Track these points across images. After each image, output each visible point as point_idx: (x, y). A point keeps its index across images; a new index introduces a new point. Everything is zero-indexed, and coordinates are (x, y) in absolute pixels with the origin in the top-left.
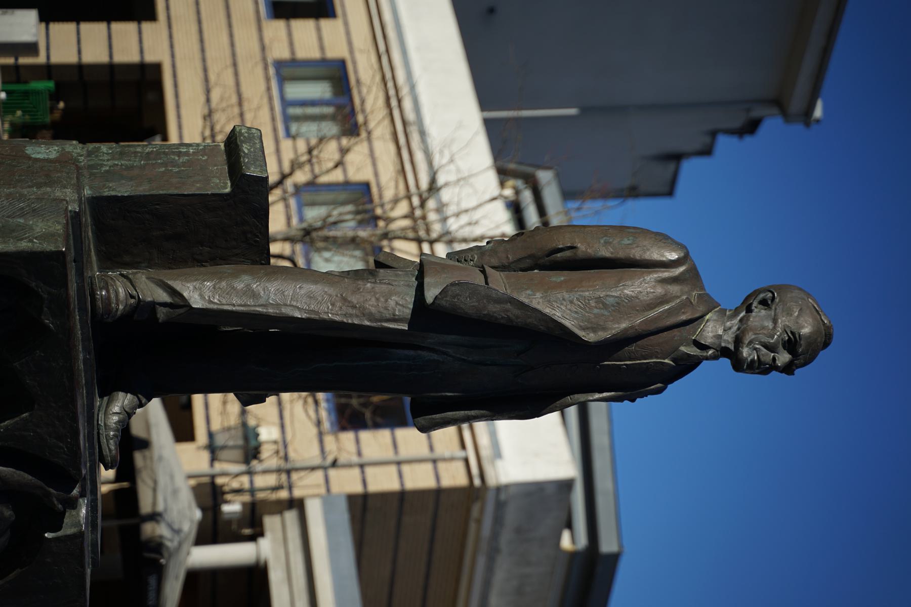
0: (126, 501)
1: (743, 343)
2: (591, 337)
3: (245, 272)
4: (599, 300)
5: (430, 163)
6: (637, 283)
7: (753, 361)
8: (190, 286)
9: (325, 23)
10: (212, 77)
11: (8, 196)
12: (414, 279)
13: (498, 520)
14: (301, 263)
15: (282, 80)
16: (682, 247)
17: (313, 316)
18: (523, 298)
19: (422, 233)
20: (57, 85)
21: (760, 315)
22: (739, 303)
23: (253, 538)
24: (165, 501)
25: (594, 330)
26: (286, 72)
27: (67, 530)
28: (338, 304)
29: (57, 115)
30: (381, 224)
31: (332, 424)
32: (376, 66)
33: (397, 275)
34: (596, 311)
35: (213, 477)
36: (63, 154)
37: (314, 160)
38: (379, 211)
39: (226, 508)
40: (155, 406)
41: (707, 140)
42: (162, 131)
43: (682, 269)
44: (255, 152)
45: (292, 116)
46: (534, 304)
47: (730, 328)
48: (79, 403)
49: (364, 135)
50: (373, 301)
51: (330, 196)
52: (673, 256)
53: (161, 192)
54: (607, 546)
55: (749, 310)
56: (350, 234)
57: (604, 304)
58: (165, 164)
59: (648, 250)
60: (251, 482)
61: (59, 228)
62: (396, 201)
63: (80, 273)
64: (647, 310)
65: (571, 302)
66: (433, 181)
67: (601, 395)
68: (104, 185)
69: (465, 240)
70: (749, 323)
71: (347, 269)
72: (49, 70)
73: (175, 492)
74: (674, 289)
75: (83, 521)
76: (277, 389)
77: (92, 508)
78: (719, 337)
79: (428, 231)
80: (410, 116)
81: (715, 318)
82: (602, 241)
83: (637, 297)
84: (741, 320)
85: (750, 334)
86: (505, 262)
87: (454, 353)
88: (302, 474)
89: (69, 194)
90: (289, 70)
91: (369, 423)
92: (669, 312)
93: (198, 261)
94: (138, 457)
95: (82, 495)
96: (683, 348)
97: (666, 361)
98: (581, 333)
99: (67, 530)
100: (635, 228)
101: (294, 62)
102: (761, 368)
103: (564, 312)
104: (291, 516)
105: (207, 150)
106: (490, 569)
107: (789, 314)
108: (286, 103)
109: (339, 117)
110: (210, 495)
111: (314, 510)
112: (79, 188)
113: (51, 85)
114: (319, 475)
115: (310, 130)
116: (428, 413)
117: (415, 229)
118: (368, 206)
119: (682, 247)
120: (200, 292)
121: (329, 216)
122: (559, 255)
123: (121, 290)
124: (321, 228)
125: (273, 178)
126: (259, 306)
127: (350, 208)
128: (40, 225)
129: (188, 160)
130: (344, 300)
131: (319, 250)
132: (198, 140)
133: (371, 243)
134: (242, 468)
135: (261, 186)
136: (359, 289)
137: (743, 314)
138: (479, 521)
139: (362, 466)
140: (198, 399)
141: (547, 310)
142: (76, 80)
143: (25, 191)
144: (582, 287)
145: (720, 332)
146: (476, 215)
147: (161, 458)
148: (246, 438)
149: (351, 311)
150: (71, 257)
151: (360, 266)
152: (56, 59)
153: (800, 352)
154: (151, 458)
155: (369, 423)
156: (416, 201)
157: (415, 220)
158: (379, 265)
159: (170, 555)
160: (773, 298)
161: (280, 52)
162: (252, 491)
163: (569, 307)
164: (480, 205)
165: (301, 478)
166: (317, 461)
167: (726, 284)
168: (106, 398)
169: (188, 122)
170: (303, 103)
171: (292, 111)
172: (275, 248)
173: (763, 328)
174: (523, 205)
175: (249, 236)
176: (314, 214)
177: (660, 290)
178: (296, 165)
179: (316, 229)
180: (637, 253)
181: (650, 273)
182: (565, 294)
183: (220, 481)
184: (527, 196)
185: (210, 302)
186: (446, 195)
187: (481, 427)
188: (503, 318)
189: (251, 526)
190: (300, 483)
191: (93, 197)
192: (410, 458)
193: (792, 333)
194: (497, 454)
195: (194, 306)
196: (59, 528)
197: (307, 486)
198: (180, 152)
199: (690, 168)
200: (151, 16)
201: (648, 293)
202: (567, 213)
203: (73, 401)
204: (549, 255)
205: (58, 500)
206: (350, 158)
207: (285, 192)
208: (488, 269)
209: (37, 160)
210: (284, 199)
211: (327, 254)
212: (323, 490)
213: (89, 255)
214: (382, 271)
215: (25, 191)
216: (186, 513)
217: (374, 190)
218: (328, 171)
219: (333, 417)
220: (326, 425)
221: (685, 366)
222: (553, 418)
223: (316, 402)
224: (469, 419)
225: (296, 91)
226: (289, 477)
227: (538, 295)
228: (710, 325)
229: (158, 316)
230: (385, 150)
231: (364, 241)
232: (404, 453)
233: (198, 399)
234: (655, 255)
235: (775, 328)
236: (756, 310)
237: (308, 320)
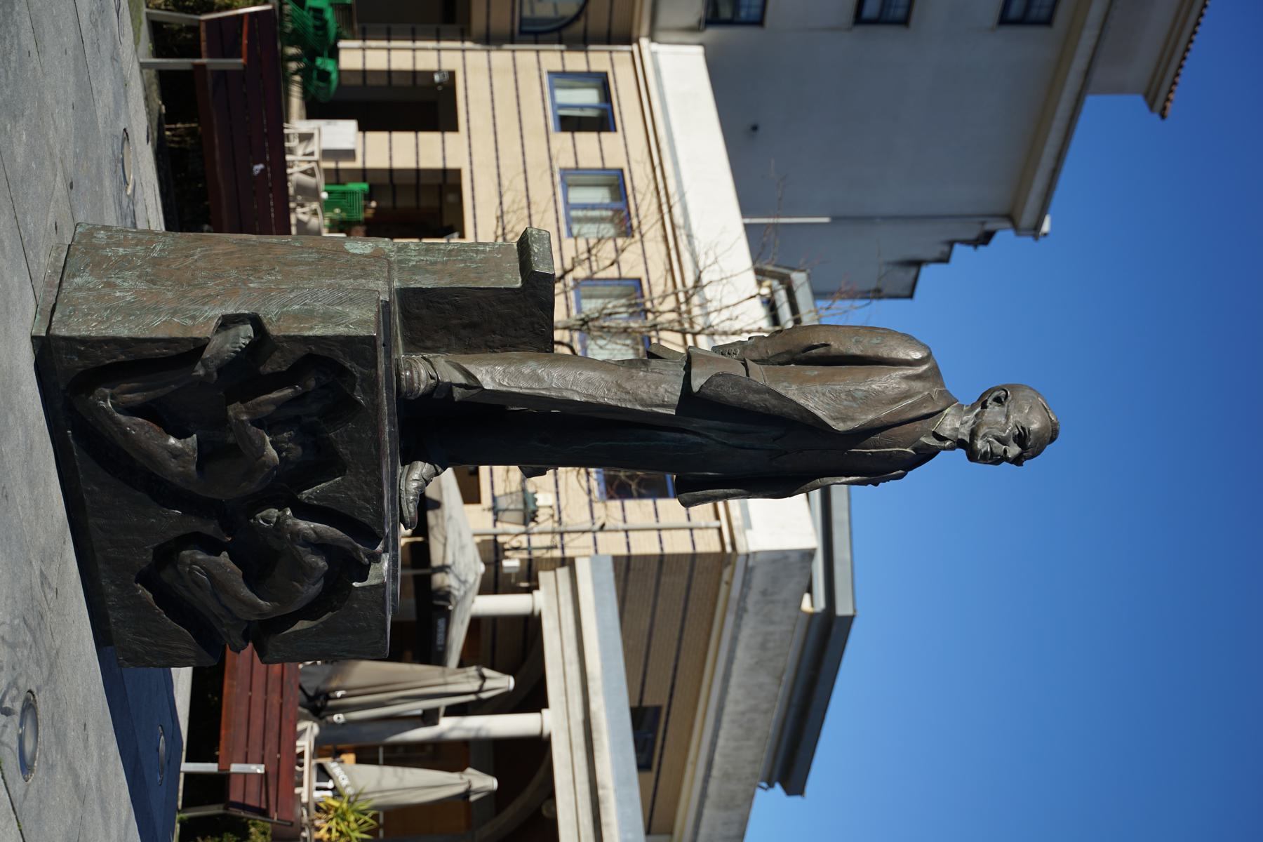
0: (420, 554)
2: (840, 427)
3: (531, 358)
5: (696, 264)
6: (884, 379)
7: (986, 452)
8: (483, 369)
10: (505, 182)
11: (329, 286)
13: (746, 584)
14: (577, 347)
15: (567, 186)
16: (926, 347)
18: (780, 390)
19: (687, 326)
20: (371, 186)
21: (993, 410)
22: (975, 400)
23: (529, 591)
24: (454, 555)
25: (844, 420)
26: (570, 178)
27: (372, 581)
28: (614, 390)
29: (370, 213)
30: (650, 316)
31: (601, 493)
32: (651, 176)
34: (845, 403)
35: (496, 535)
36: (376, 249)
37: (593, 258)
38: (648, 305)
39: (506, 563)
40: (448, 476)
41: (946, 248)
42: (457, 227)
43: (925, 367)
45: (573, 217)
46: (790, 396)
48: (384, 470)
49: (637, 236)
50: (645, 388)
51: (607, 290)
52: (917, 355)
54: (843, 609)
55: (984, 406)
56: (623, 325)
57: (853, 397)
58: (463, 261)
60: (529, 541)
61: (371, 316)
62: (664, 296)
63: (388, 355)
65: (824, 394)
66: (698, 279)
69: (725, 333)
71: (619, 358)
72: (364, 174)
73: (462, 548)
74: (917, 385)
75: (385, 574)
76: (556, 465)
77: (394, 562)
78: (957, 430)
79: (692, 323)
80: (679, 220)
86: (765, 356)
87: (719, 436)
88: (573, 536)
89: (381, 285)
90: (572, 177)
91: (635, 493)
92: (912, 406)
94: (431, 515)
95: (385, 550)
96: (923, 439)
99: (372, 581)
102: (993, 459)
104: (563, 572)
105: (504, 249)
106: (738, 626)
107: (1021, 411)
108: (569, 206)
109: (617, 221)
110: (493, 551)
111: (583, 567)
112: (389, 280)
113: (365, 186)
114: (589, 536)
115: (591, 230)
116: (691, 489)
117: (680, 323)
118: (639, 301)
119: (926, 347)
120: (494, 375)
121: (604, 309)
123: (423, 371)
124: (597, 318)
125: (558, 273)
127: (623, 301)
128: (356, 312)
130: (619, 386)
131: (594, 338)
132: (491, 239)
133: (641, 333)
134: (522, 529)
135: (548, 281)
138: (729, 584)
139: (626, 531)
140: (484, 470)
141: (802, 401)
142: (385, 183)
143: (343, 282)
145: (958, 425)
147: (450, 518)
148: (525, 503)
149: (627, 397)
150: (380, 342)
151: (630, 355)
152: (370, 164)
153: (1028, 445)
154: (443, 517)
155: (635, 493)
156: (682, 297)
157: (680, 314)
158: (651, 355)
159: (457, 604)
160: (1007, 396)
162: (529, 549)
165: (573, 540)
166: (588, 526)
167: (965, 387)
169: (482, 222)
170: (585, 207)
171: (574, 213)
172: (558, 335)
173: (997, 423)
174: (778, 304)
176: (591, 306)
177: (904, 386)
178: (576, 262)
179: (593, 320)
180: (884, 352)
183: (501, 539)
184: (782, 296)
185: (500, 384)
186: (708, 292)
187: (733, 503)
189: (528, 580)
190: (571, 544)
192: (667, 526)
194: (748, 525)
196: (364, 578)
197: (577, 546)
200: (454, 128)
202: (817, 312)
203: (379, 467)
206: (624, 257)
207: (565, 285)
208: (749, 363)
209: (354, 255)
210: (565, 292)
211: (602, 342)
212: (592, 551)
213: (396, 340)
214: (653, 361)
215: (343, 282)
216: (470, 567)
217: (645, 286)
218: (605, 268)
219: (603, 487)
220: (596, 493)
221: (924, 455)
222: (801, 497)
223: (588, 474)
224: (726, 497)
225: (578, 196)
226: (562, 538)
227: (794, 387)
228: (949, 419)
231: (634, 331)
232: (664, 522)
233: (484, 470)
234: (901, 354)
237: (587, 403)
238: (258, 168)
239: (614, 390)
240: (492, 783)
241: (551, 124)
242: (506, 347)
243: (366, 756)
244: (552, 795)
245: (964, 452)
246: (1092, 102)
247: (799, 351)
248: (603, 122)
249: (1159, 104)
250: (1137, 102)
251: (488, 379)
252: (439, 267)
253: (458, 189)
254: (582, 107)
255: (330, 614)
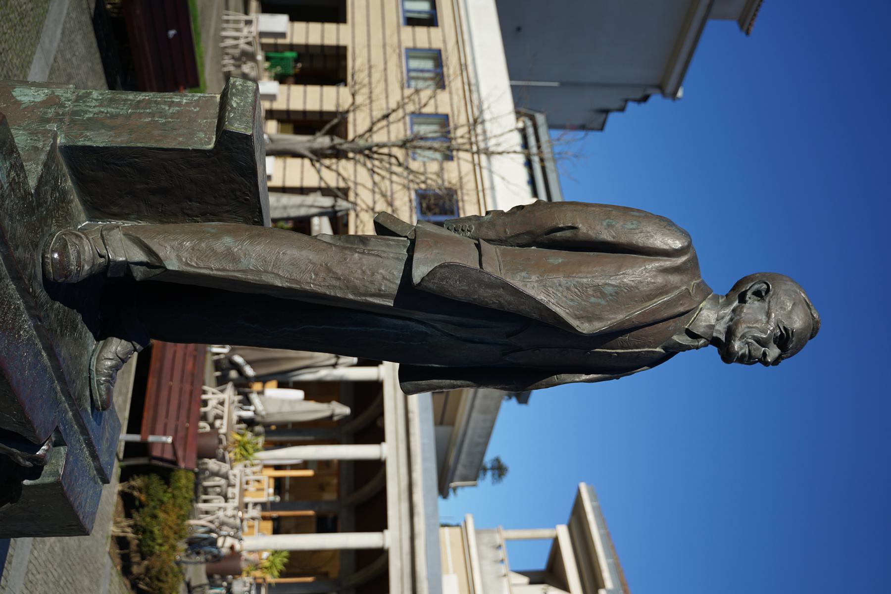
1: (735, 336)
2: (585, 328)
3: (228, 232)
4: (598, 289)
7: (743, 355)
9: (433, 30)
12: (405, 250)
15: (408, 57)
17: (294, 286)
21: (753, 306)
25: (590, 319)
28: (322, 275)
29: (297, 70)
33: (388, 246)
34: (593, 300)
41: (622, 104)
43: (683, 259)
44: (244, 106)
47: (723, 318)
52: (678, 244)
53: (139, 145)
55: (742, 299)
57: (602, 292)
58: (152, 115)
59: (652, 237)
64: (646, 301)
67: (588, 377)
68: (82, 134)
70: (743, 315)
72: (291, 47)
74: (674, 279)
78: (712, 327)
80: (473, 81)
81: (709, 306)
82: (605, 224)
83: (637, 288)
84: (734, 311)
85: (744, 326)
86: (502, 236)
90: (413, 53)
92: (667, 304)
93: (188, 215)
96: (676, 338)
97: (658, 349)
98: (574, 323)
100: (638, 211)
101: (415, 49)
102: (747, 359)
103: (560, 298)
115: (421, 84)
119: (685, 234)
122: (558, 234)
124: (412, 140)
126: (238, 271)
129: (178, 111)
130: (329, 270)
136: (345, 259)
137: (736, 303)
141: (541, 297)
142: (305, 52)
144: (580, 272)
146: (501, 139)
149: (334, 282)
160: (768, 291)
161: (408, 42)
163: (565, 294)
164: (502, 135)
168: (101, 342)
173: (757, 321)
175: (238, 193)
177: (660, 280)
180: (639, 239)
181: (652, 261)
182: (562, 279)
184: (530, 131)
188: (493, 303)
191: (66, 147)
193: (784, 328)
195: (170, 267)
198: (173, 102)
199: (613, 117)
201: (648, 283)
204: (548, 233)
205: (23, 458)
208: (484, 244)
221: (672, 351)
225: (414, 64)
227: (534, 278)
229: (135, 275)
230: (458, 99)
235: (768, 322)
236: (750, 301)
237: (290, 289)
238: (172, 33)
239: (322, 275)
240: (347, 410)
241: (402, 21)
242: (189, 216)
243: (281, 385)
244: (381, 414)
245: (716, 349)
246: (711, 24)
247: (538, 231)
248: (431, 21)
249: (745, 27)
250: (734, 25)
251: (173, 256)
252: (119, 121)
253: (345, 57)
254: (420, 12)
255: (8, 504)
